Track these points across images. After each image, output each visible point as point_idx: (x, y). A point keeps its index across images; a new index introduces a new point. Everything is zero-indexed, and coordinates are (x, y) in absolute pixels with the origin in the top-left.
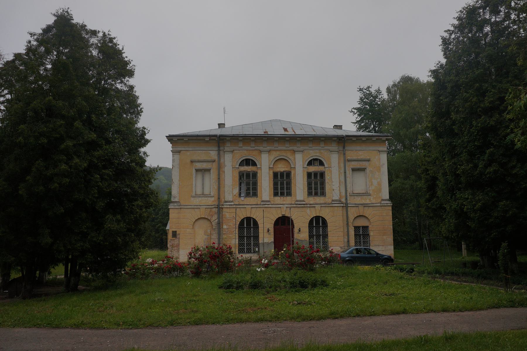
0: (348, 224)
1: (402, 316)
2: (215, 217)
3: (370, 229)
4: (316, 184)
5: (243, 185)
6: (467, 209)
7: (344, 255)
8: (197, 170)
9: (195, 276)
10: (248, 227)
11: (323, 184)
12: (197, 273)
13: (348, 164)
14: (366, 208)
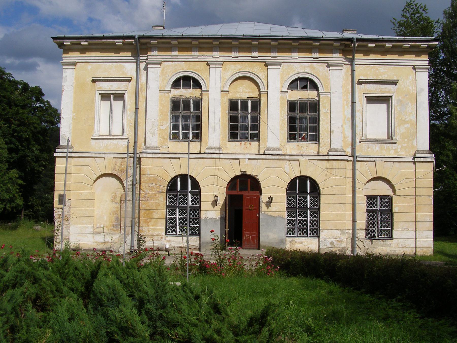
11: (315, 121)
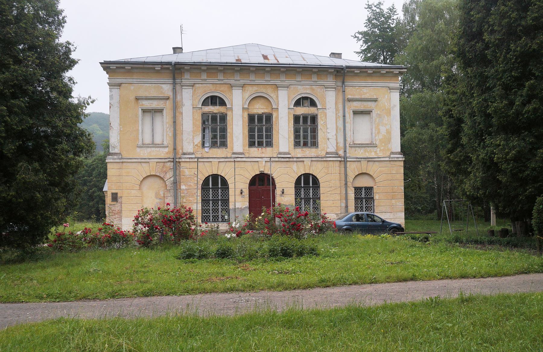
0: (346, 184)
1: (410, 283)
2: (170, 174)
3: (375, 190)
4: (305, 131)
5: (207, 131)
6: (498, 158)
7: (340, 223)
8: (144, 111)
9: (143, 247)
10: (215, 186)
11: (314, 131)
12: (146, 242)
13: (348, 104)
14: (371, 164)
